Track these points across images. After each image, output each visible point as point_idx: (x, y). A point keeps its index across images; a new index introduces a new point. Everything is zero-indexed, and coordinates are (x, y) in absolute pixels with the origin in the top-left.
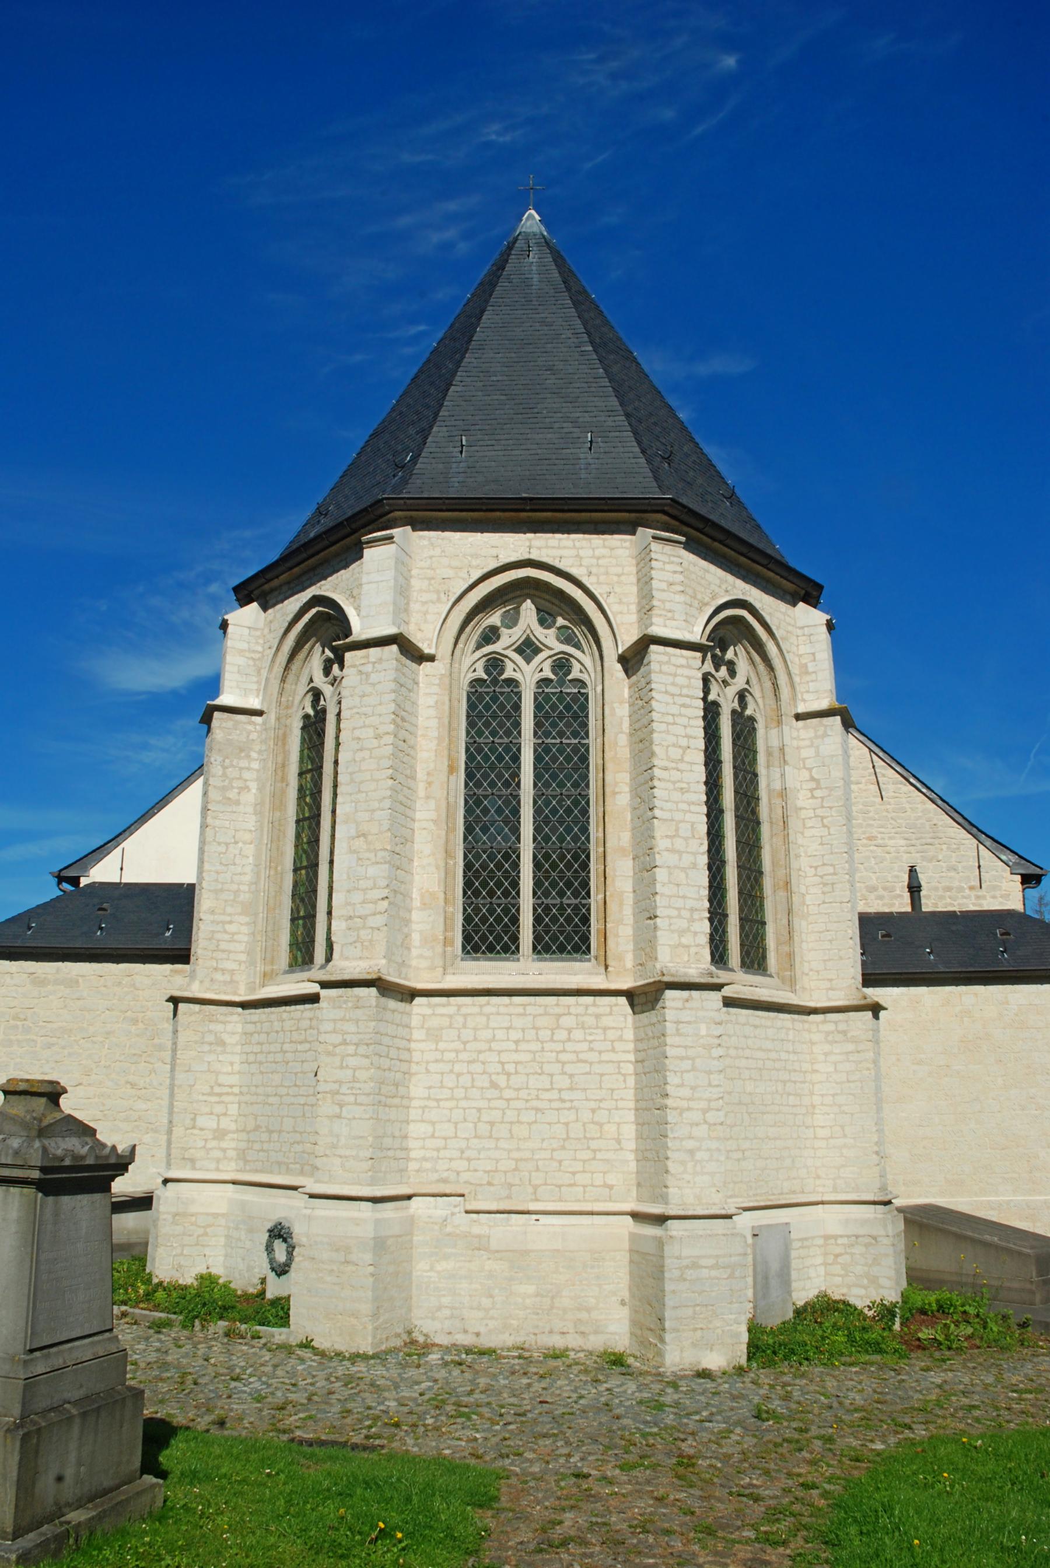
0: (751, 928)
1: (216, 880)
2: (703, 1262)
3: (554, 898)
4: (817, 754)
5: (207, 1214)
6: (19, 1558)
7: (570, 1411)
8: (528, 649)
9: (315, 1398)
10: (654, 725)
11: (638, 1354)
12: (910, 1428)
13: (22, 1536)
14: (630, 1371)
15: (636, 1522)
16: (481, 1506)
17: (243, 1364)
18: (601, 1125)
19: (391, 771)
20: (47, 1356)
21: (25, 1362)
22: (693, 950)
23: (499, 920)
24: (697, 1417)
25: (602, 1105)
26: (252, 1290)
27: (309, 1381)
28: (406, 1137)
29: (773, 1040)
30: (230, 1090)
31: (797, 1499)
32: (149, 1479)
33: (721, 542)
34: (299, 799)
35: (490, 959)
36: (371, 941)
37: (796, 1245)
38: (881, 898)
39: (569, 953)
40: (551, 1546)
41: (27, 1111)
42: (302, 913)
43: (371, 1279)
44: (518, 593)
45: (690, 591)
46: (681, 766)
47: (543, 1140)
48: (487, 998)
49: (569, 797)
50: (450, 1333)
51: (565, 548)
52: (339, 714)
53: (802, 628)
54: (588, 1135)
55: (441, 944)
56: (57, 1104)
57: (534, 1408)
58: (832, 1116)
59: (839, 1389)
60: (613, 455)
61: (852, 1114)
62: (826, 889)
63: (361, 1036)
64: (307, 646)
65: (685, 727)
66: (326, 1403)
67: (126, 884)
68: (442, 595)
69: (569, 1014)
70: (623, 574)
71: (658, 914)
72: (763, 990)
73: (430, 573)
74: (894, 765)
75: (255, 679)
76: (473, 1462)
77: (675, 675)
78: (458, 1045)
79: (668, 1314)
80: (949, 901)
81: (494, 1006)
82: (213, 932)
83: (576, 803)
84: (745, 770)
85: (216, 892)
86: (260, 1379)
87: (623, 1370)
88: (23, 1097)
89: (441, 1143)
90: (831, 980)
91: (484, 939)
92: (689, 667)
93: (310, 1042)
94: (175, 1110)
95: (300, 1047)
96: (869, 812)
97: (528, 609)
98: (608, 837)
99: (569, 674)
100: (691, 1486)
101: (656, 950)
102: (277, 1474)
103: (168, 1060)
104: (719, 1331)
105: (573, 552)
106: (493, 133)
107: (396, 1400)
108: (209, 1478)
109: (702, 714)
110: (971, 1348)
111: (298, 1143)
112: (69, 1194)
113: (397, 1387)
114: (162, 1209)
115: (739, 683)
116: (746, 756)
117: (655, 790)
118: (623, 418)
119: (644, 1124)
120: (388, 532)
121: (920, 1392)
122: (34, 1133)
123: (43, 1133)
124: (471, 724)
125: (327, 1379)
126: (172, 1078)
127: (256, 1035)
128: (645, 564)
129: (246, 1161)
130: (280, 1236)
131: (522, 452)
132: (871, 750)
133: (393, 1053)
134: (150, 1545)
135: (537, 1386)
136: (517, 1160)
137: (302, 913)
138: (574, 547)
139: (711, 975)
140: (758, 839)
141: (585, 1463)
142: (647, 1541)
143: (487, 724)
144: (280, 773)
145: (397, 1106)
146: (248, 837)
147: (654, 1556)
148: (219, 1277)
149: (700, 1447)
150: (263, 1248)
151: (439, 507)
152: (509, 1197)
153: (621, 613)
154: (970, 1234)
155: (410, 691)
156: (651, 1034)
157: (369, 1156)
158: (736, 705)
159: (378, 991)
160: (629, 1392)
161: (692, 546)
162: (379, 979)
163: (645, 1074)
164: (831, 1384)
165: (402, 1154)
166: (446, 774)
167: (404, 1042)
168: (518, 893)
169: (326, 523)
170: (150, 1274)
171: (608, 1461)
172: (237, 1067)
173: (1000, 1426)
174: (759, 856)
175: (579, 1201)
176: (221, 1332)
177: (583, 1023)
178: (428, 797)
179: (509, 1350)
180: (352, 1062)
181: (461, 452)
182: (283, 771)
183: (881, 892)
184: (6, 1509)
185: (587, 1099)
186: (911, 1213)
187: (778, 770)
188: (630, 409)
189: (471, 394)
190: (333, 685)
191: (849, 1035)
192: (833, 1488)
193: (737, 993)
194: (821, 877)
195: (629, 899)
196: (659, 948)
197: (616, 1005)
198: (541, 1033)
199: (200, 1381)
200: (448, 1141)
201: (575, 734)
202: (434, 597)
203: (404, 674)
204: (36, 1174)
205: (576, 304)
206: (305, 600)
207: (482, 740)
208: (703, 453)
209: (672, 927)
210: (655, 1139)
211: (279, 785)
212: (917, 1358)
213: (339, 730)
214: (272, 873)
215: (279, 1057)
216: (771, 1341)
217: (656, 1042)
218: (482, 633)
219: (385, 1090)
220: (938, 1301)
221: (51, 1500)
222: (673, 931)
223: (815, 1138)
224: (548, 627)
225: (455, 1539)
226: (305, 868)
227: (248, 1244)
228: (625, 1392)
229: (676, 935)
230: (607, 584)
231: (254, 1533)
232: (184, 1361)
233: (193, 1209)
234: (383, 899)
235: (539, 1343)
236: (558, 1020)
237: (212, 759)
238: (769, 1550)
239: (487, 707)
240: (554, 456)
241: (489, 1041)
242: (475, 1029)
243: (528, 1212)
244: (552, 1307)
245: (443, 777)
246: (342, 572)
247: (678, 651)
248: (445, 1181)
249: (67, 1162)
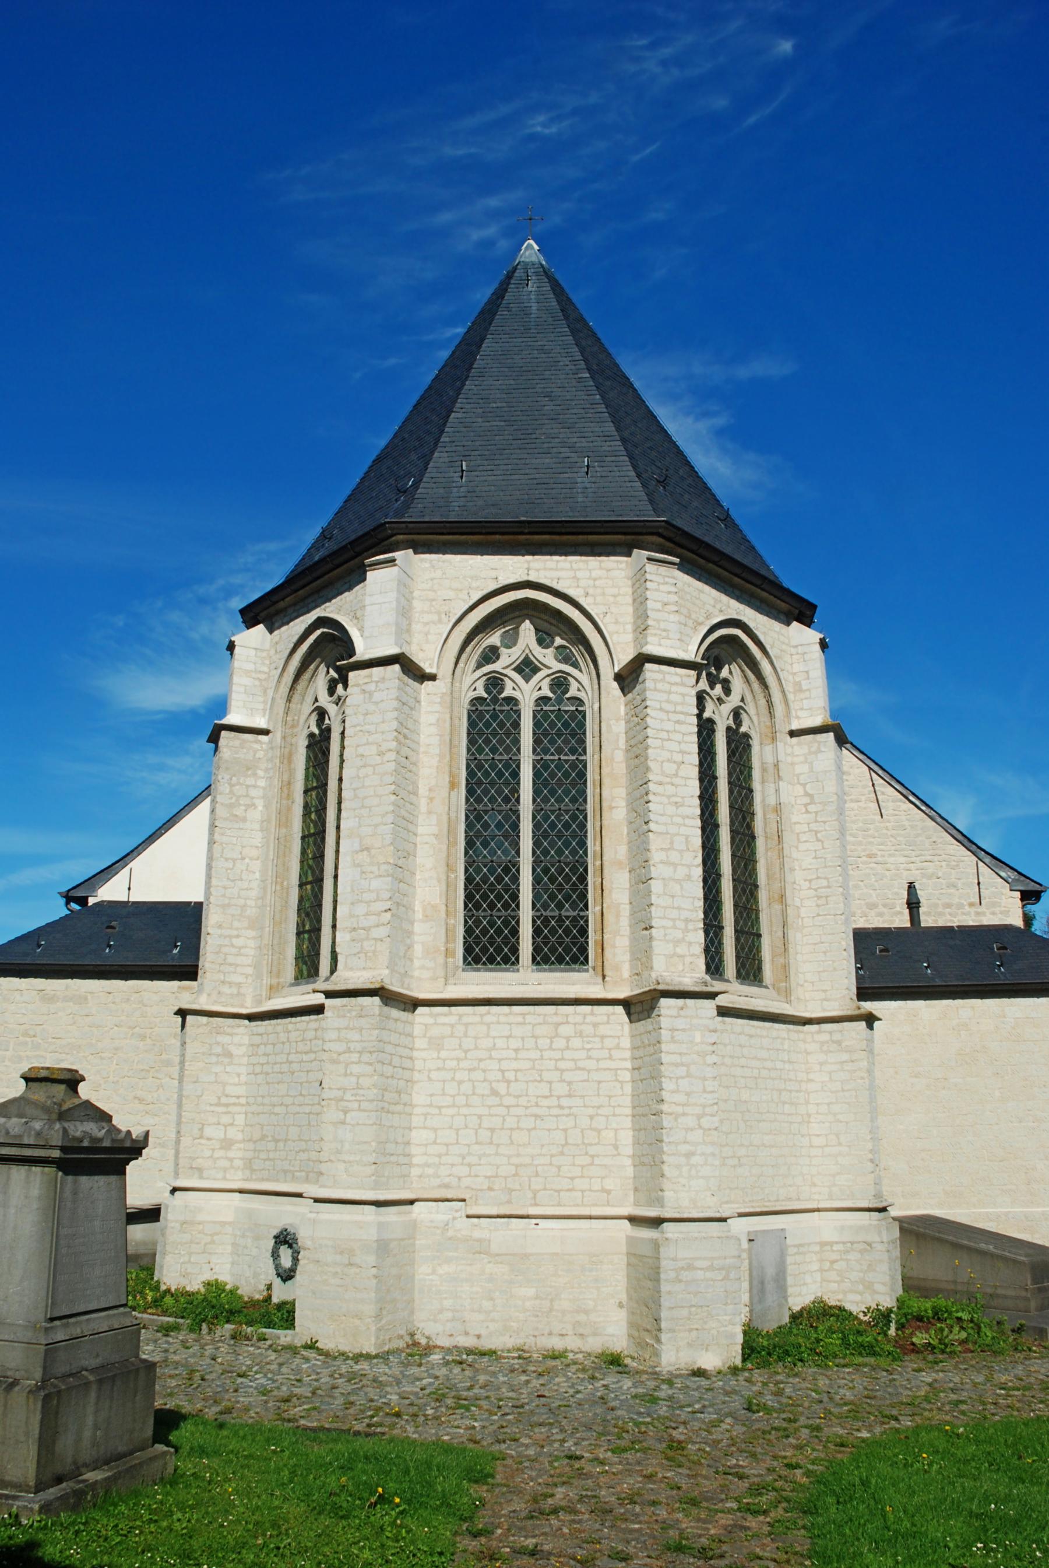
0: (747, 941)
1: (224, 896)
2: (699, 1264)
3: (552, 910)
4: (811, 770)
5: (215, 1222)
6: (41, 1508)
7: (565, 1403)
8: (527, 668)
9: (319, 1392)
10: (649, 741)
11: (636, 1355)
12: (896, 1419)
13: (44, 1490)
14: (627, 1370)
15: (624, 1495)
16: (476, 1482)
17: (249, 1363)
18: (599, 1131)
19: (393, 787)
20: (67, 1325)
21: (47, 1329)
22: (688, 960)
23: (499, 932)
24: (690, 1409)
25: (600, 1112)
26: (258, 1297)
27: (313, 1377)
28: (408, 1143)
29: (768, 1049)
30: (237, 1101)
31: (780, 1477)
32: (161, 1448)
33: (715, 563)
34: (304, 815)
35: (491, 970)
36: (374, 951)
37: (791, 1251)
38: (881, 915)
39: (568, 963)
40: (541, 1513)
41: (48, 1097)
42: (307, 927)
43: (375, 1281)
45: (684, 611)
46: (676, 781)
47: (543, 1146)
49: (567, 812)
50: (451, 1335)
51: (562, 569)
52: (343, 733)
53: (796, 647)
54: (586, 1141)
56: (76, 1092)
57: (532, 1401)
58: (827, 1124)
59: (831, 1386)
60: (610, 479)
61: (847, 1123)
62: (819, 902)
63: (364, 1044)
64: (312, 667)
65: (679, 742)
66: (330, 1396)
67: (134, 903)
68: (443, 616)
69: (568, 1023)
70: (619, 594)
71: (653, 924)
72: (758, 1000)
74: (893, 783)
75: (261, 699)
76: (471, 1446)
78: (460, 1054)
79: (664, 1314)
80: (949, 917)
81: (494, 1015)
82: (220, 946)
83: (574, 817)
84: (740, 786)
85: (224, 906)
86: (265, 1376)
87: (620, 1369)
88: (44, 1084)
89: (443, 1150)
90: (825, 991)
91: (485, 950)
92: (683, 684)
93: (315, 1052)
94: (183, 1120)
95: (305, 1057)
96: (868, 829)
97: (527, 629)
98: (605, 850)
99: (567, 692)
100: (680, 1466)
101: (651, 960)
102: (282, 1451)
103: (176, 1076)
104: (714, 1332)
105: (571, 574)
106: (538, 124)
107: (398, 1394)
108: (217, 1453)
109: (696, 730)
110: (965, 1352)
111: (303, 1151)
112: (87, 1175)
113: (398, 1382)
114: (170, 1217)
115: (734, 700)
116: (742, 772)
117: (650, 804)
118: (619, 443)
119: (641, 1130)
120: (390, 555)
121: (910, 1389)
122: (54, 1116)
123: (62, 1116)
124: (472, 741)
125: (331, 1376)
126: (181, 1088)
127: (262, 1047)
128: (641, 585)
129: (253, 1170)
130: (285, 1242)
131: (522, 477)
132: (870, 768)
133: (396, 1061)
134: (161, 1502)
135: (536, 1383)
136: (517, 1166)
137: (307, 927)
138: (572, 569)
139: (705, 984)
140: (753, 853)
141: (579, 1447)
142: (633, 1510)
143: (487, 741)
144: (285, 791)
145: (400, 1113)
146: (254, 853)
147: (640, 1523)
148: (226, 1284)
149: (691, 1434)
150: (269, 1254)
151: (439, 531)
152: (509, 1202)
154: (965, 1242)
155: (412, 709)
156: (646, 1042)
157: (373, 1161)
158: (731, 722)
160: (625, 1388)
161: (688, 567)
162: (382, 988)
163: (641, 1081)
164: (823, 1382)
165: (405, 1160)
166: (447, 790)
167: (407, 1050)
168: (518, 906)
169: (330, 546)
170: (158, 1282)
171: (600, 1446)
172: (243, 1078)
173: (985, 1418)
174: (754, 869)
175: (578, 1205)
176: (228, 1335)
177: (581, 1032)
178: (429, 812)
179: (509, 1351)
180: (355, 1069)
181: (462, 477)
182: (289, 789)
183: (881, 909)
184: (28, 1464)
185: (585, 1106)
186: (908, 1223)
187: (772, 785)
188: (626, 434)
189: (471, 420)
190: (337, 704)
191: (844, 1045)
192: (816, 1467)
193: (733, 1003)
194: (816, 890)
195: (626, 910)
196: (654, 957)
197: (614, 1014)
198: (540, 1041)
199: (207, 1377)
200: (450, 1147)
201: (573, 751)
202: (435, 617)
203: (406, 693)
204: (56, 1154)
205: (574, 332)
206: (310, 622)
207: (482, 757)
208: (699, 477)
210: (651, 1144)
211: (284, 802)
212: (911, 1361)
213: (343, 747)
214: (278, 888)
215: (285, 1068)
216: (765, 1343)
217: (651, 1050)
218: (482, 652)
219: (388, 1096)
220: (934, 1308)
221: (69, 1460)
223: (811, 1146)
224: (547, 647)
225: (449, 1506)
226: (311, 883)
227: (255, 1252)
228: (621, 1388)
230: (604, 605)
231: (259, 1497)
232: (192, 1360)
233: (200, 1217)
234: (386, 911)
235: (539, 1345)
236: (556, 1030)
237: (220, 777)
238: (750, 1517)
239: (488, 725)
240: (552, 481)
241: (489, 1050)
242: (476, 1038)
243: (528, 1217)
244: (551, 1310)
246: (346, 594)
247: (672, 669)
248: (447, 1186)
249: (86, 1143)
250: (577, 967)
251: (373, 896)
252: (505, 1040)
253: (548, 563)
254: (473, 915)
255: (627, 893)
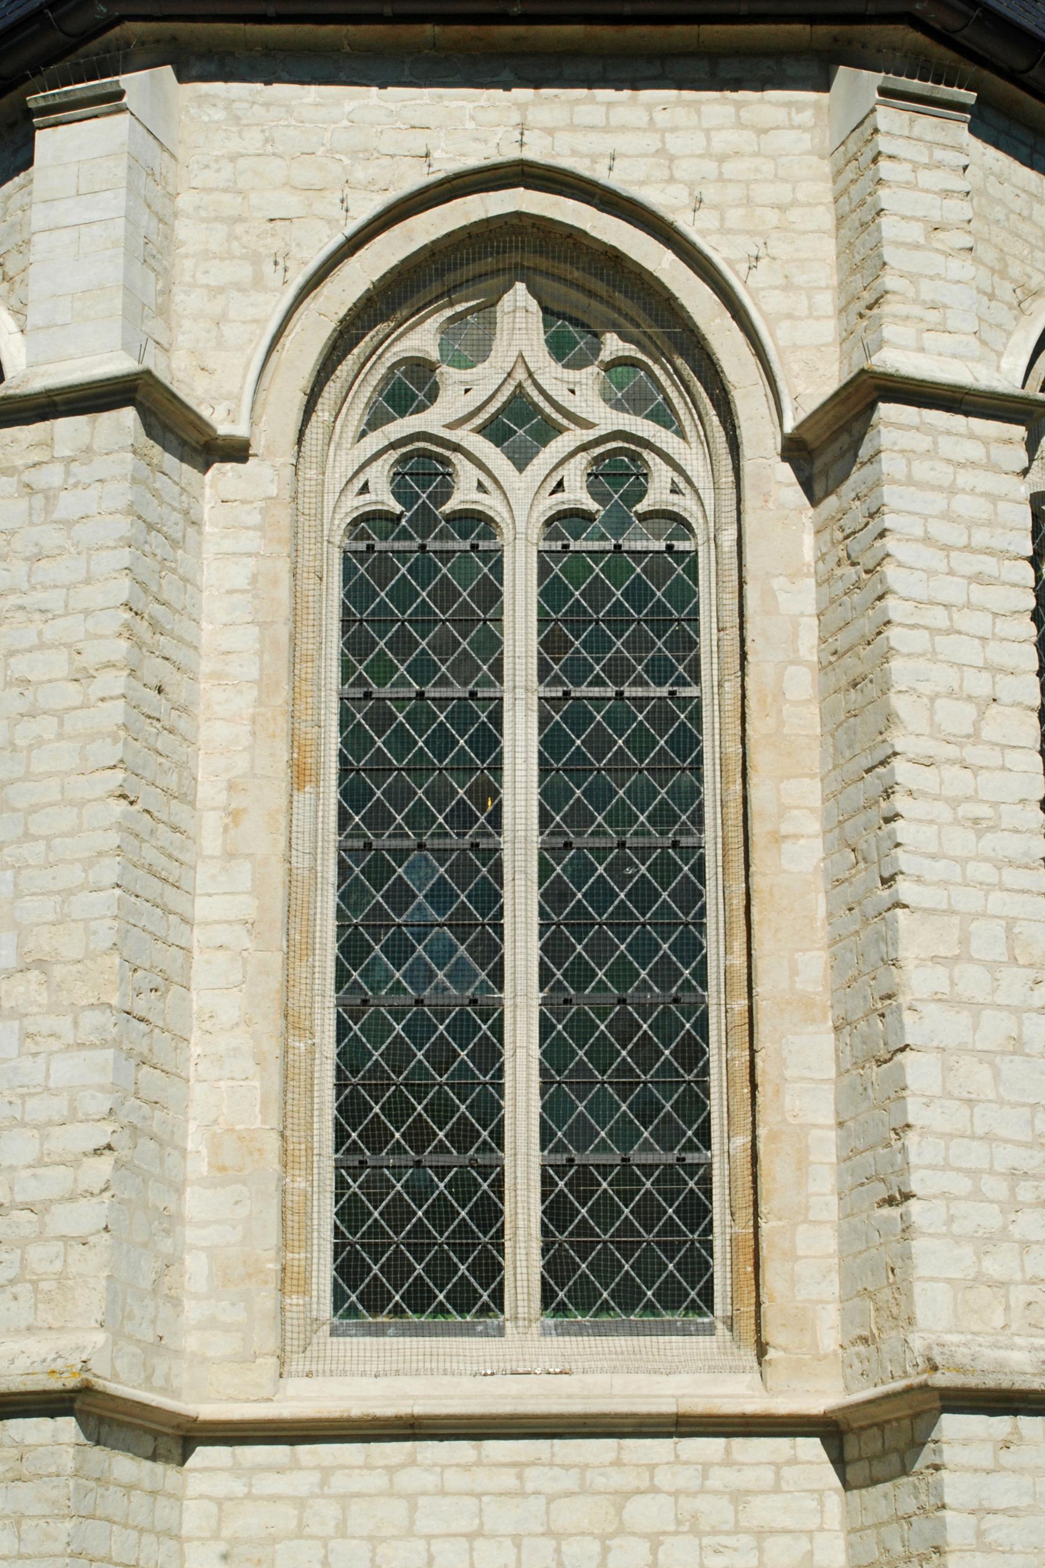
3: (603, 1147)
19: (119, 775)
22: (1019, 1295)
23: (441, 1214)
35: (418, 1331)
36: (61, 1277)
39: (650, 1308)
44: (489, 263)
45: (989, 255)
46: (975, 754)
48: (408, 1445)
49: (643, 853)
51: (623, 128)
55: (273, 1285)
69: (654, 1490)
70: (794, 203)
71: (914, 1187)
73: (231, 204)
77: (952, 490)
81: (429, 1468)
83: (665, 870)
91: (397, 1270)
92: (991, 467)
98: (759, 964)
101: (909, 1296)
117: (898, 825)
143: (402, 644)
153: (789, 316)
155: (175, 544)
156: (898, 1548)
159: (83, 1425)
162: (86, 1390)
166: (284, 785)
168: (498, 1136)
178: (230, 855)
196: (918, 1287)
197: (793, 1461)
201: (660, 672)
202: (244, 272)
203: (155, 493)
207: (386, 691)
209: (955, 1228)
218: (386, 379)
222: (958, 1239)
229: (967, 1250)
234: (97, 1152)
236: (620, 1509)
239: (403, 595)
245: (276, 794)
247: (958, 421)
250: (677, 1317)
251: (58, 1107)
252: (464, 1543)
253: (581, 109)
254: (363, 1164)
255: (829, 1093)
